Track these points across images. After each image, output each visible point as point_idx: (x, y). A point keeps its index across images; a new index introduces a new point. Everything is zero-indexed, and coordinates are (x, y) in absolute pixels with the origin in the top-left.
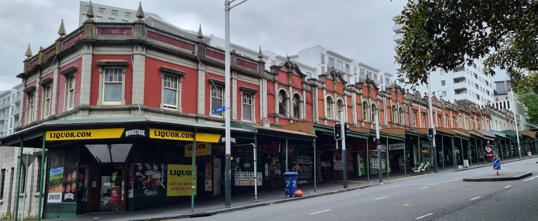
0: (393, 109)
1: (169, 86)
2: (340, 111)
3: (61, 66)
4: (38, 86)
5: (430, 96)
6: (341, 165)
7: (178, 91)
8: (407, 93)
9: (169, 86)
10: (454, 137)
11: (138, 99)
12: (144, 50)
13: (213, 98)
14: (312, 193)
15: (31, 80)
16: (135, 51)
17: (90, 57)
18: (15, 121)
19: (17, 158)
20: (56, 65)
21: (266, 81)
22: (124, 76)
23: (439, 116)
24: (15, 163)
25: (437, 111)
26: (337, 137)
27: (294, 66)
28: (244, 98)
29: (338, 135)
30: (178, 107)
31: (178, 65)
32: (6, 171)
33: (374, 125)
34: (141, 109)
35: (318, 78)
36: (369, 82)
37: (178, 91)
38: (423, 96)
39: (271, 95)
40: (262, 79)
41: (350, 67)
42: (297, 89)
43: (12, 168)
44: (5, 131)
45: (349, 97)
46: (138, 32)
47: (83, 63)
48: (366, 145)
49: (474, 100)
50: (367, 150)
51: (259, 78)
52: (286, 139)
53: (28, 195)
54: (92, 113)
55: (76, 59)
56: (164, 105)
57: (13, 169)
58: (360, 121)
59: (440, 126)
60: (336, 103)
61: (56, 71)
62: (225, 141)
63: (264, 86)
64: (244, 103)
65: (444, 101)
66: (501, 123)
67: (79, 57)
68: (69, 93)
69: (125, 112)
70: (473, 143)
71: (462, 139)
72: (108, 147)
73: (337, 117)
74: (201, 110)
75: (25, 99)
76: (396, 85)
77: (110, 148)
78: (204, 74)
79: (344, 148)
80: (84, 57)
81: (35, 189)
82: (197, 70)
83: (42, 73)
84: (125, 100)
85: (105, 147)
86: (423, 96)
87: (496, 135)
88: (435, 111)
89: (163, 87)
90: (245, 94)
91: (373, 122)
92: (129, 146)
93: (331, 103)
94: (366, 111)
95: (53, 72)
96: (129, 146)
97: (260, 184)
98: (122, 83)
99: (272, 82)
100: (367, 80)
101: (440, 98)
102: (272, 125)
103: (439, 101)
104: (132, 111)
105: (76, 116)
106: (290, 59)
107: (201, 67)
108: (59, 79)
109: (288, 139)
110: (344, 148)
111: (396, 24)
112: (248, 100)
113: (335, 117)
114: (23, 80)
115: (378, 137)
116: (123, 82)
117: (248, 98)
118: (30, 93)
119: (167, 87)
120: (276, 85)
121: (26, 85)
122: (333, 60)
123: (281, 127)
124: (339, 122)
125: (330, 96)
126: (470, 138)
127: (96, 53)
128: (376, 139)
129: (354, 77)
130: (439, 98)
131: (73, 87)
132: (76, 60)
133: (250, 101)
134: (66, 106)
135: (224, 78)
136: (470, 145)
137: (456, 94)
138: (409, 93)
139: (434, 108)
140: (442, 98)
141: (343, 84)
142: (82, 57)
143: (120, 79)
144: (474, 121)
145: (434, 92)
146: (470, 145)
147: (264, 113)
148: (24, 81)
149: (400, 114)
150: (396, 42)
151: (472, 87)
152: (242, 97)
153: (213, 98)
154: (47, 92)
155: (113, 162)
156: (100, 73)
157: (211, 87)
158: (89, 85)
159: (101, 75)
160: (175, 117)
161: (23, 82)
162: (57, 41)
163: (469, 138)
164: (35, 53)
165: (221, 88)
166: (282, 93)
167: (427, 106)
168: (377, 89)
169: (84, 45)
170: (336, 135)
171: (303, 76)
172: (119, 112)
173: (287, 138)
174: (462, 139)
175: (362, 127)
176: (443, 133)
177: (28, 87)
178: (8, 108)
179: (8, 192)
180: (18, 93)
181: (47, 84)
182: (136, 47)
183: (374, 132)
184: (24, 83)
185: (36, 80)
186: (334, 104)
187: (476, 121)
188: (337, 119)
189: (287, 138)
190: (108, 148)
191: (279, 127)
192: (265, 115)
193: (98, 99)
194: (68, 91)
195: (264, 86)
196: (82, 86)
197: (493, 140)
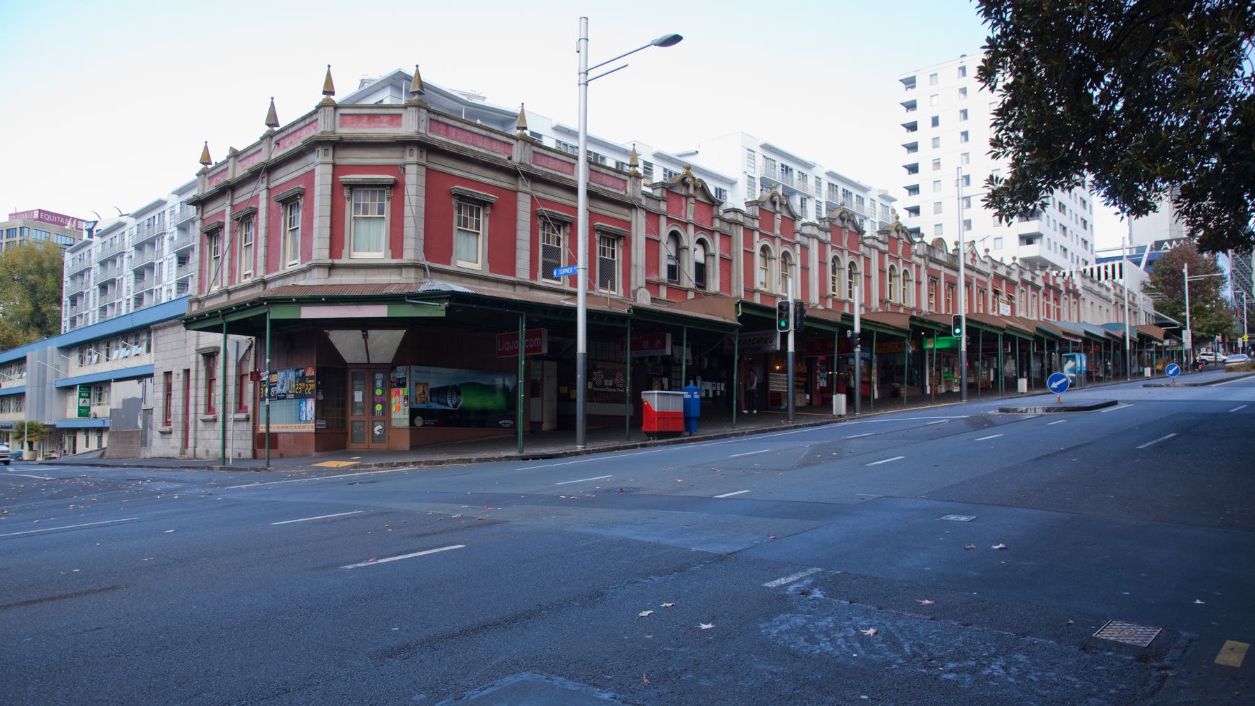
0: (890, 274)
1: (465, 226)
2: (786, 275)
3: (272, 185)
4: (227, 220)
5: (964, 249)
6: (783, 382)
7: (481, 234)
8: (919, 242)
9: (465, 226)
10: (1004, 333)
11: (411, 251)
12: (425, 154)
13: (544, 245)
14: (728, 431)
15: (212, 210)
16: (409, 159)
17: (329, 169)
18: (136, 282)
19: (195, 352)
20: (262, 183)
21: (644, 213)
22: (387, 206)
23: (980, 291)
24: (192, 360)
25: (977, 280)
26: (781, 328)
27: (700, 184)
28: (602, 246)
29: (783, 324)
30: (477, 265)
31: (481, 183)
32: (173, 376)
33: (852, 306)
34: (429, 269)
35: (744, 208)
36: (846, 217)
37: (481, 234)
38: (951, 248)
39: (652, 245)
40: (637, 208)
41: (865, 201)
42: (703, 229)
43: (184, 370)
44: (118, 301)
45: (726, 237)
46: (411, 117)
47: (317, 180)
48: (834, 343)
49: (1054, 257)
50: (834, 354)
51: (631, 207)
52: (683, 328)
53: (220, 419)
54: (333, 272)
55: (301, 172)
56: (462, 263)
57: (187, 372)
58: (823, 298)
59: (981, 311)
60: (778, 259)
61: (263, 194)
62: (103, 297)
63: (639, 222)
64: (602, 256)
65: (992, 260)
66: (1094, 304)
67: (307, 169)
68: (289, 236)
69: (392, 271)
70: (1041, 347)
71: (1019, 338)
72: (363, 335)
73: (780, 287)
74: (523, 273)
75: (202, 245)
76: (899, 224)
77: (365, 337)
78: (527, 199)
79: (791, 348)
80: (318, 170)
81: (232, 406)
82: (516, 192)
83: (235, 197)
84: (390, 248)
85: (357, 334)
86: (951, 248)
87: (1086, 332)
88: (972, 280)
89: (456, 227)
90: (604, 238)
91: (850, 299)
92: (400, 334)
93: (769, 259)
94: (837, 276)
95: (257, 192)
96: (400, 334)
97: (632, 414)
98: (384, 217)
99: (653, 216)
100: (897, 226)
101: (985, 254)
102: (653, 300)
103: (982, 259)
104: (404, 270)
105: (305, 278)
106: (690, 171)
107: (524, 186)
108: (269, 208)
109: (688, 329)
110: (791, 348)
111: (907, 89)
112: (608, 250)
113: (777, 289)
114: (197, 209)
115: (857, 329)
116: (387, 214)
117: (609, 246)
118: (212, 233)
119: (462, 228)
120: (663, 220)
121: (204, 217)
122: (835, 188)
123: (673, 304)
124: (783, 298)
125: (701, 238)
126: (1035, 337)
127: (339, 162)
128: (853, 334)
129: (870, 221)
130: (982, 254)
131: (299, 225)
132: (302, 175)
133: (613, 251)
134: (284, 259)
135: (575, 210)
136: (1034, 349)
137: (1021, 244)
138: (924, 242)
139: (970, 273)
140: (989, 254)
141: (858, 234)
142: (314, 170)
143: (381, 211)
144: (1048, 303)
145: (974, 242)
146: (1034, 349)
147: (639, 277)
148: (200, 211)
149: (904, 285)
150: (906, 127)
151: (1047, 227)
152: (598, 246)
153: (600, 258)
154: (246, 232)
155: (371, 362)
156: (346, 200)
157: (541, 225)
158: (327, 222)
159: (348, 204)
160: (477, 282)
161: (197, 213)
162: (263, 139)
163: (1034, 337)
164: (218, 156)
165: (608, 239)
166: (675, 236)
167: (957, 270)
168: (860, 232)
169: (318, 147)
170: (780, 324)
171: (717, 203)
172: (381, 271)
173: (686, 327)
174: (1019, 338)
175: (826, 309)
176: (982, 324)
177: (208, 223)
178: (122, 254)
179: (180, 412)
180: (138, 225)
181: (246, 218)
182: (411, 150)
183: (850, 318)
184: (200, 215)
185: (224, 210)
186: (774, 261)
187: (1051, 303)
188: (780, 292)
189: (686, 327)
190: (364, 338)
191: (670, 304)
192: (642, 282)
193: (343, 248)
194: (287, 231)
195: (639, 222)
196: (316, 223)
197: (1080, 341)
